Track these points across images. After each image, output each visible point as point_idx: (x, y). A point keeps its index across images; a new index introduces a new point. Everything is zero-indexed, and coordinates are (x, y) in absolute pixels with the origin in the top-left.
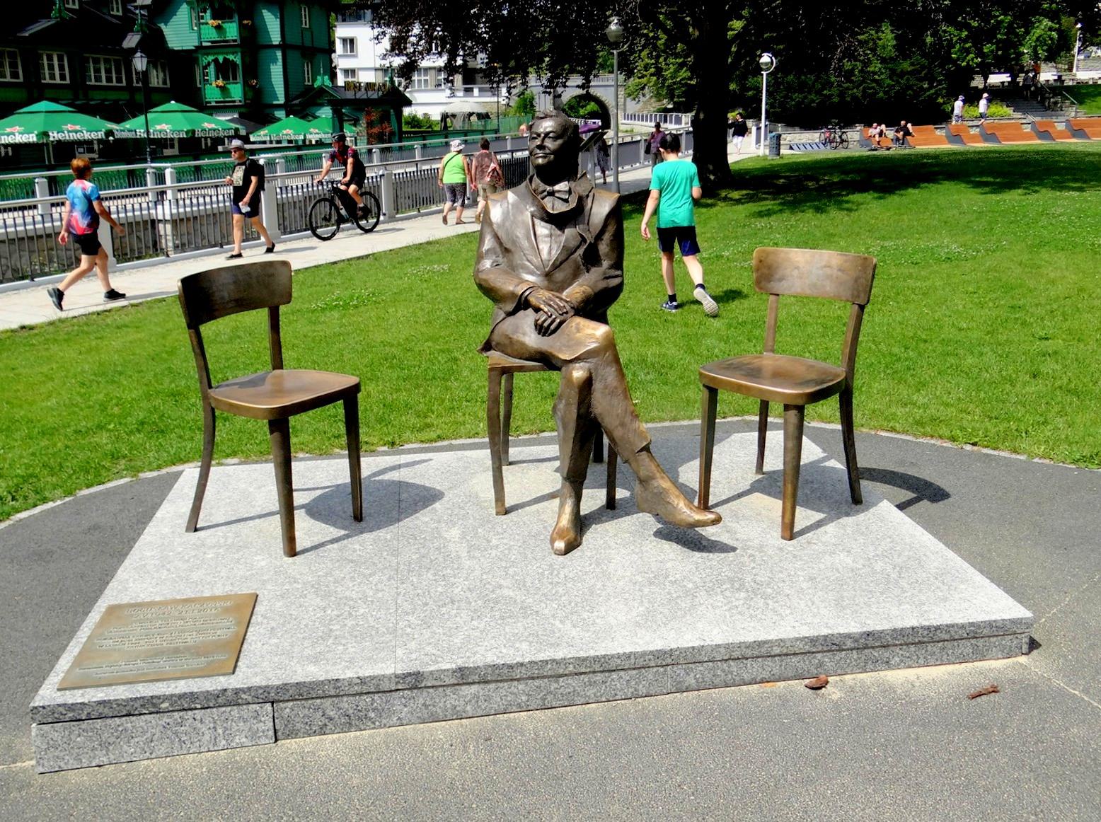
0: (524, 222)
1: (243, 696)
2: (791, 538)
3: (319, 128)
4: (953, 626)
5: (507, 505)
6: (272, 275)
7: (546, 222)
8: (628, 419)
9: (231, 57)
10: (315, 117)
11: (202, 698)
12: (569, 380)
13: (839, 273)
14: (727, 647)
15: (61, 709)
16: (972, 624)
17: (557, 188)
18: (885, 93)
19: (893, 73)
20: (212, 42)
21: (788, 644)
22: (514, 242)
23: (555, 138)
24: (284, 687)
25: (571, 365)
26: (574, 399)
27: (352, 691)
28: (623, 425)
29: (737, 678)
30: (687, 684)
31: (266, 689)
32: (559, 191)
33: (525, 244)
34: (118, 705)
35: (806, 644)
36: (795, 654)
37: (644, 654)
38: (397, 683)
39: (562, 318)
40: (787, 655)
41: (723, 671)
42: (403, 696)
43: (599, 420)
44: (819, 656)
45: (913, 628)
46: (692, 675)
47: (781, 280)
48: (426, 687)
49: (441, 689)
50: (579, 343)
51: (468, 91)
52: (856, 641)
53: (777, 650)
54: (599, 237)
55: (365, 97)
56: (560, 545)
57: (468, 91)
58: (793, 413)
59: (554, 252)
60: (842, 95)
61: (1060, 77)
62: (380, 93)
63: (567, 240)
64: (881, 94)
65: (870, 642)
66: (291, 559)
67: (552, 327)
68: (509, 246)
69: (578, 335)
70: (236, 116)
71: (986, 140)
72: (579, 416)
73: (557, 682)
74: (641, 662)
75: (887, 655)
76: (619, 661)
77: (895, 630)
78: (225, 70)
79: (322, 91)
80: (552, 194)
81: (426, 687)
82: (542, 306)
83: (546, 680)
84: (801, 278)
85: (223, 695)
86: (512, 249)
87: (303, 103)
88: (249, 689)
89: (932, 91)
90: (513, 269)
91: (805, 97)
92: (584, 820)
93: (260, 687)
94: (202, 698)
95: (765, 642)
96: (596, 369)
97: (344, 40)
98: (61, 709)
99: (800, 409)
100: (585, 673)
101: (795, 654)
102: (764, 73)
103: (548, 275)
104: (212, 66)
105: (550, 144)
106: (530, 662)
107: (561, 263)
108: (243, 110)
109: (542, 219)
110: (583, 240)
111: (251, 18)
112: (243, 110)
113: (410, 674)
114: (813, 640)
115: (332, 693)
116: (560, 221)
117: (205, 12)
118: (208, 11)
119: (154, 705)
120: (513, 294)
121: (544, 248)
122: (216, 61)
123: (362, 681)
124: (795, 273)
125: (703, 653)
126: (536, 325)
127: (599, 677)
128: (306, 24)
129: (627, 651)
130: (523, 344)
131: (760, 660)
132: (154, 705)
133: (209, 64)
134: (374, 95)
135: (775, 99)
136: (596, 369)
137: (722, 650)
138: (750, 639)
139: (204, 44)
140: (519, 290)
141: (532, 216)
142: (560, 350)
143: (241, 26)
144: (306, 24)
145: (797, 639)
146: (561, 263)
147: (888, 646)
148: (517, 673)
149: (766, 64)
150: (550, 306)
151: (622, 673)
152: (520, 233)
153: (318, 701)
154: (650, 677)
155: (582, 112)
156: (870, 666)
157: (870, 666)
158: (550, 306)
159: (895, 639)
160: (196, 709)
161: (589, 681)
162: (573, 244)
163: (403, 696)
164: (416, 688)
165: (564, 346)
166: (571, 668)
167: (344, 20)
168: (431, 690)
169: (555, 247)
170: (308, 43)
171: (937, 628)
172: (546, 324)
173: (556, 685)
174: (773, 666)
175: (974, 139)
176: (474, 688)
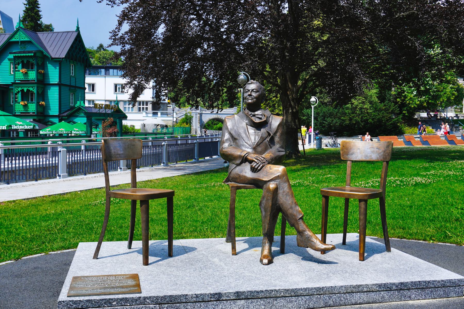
0: (243, 127)
1: (148, 301)
2: (363, 260)
3: (79, 126)
4: (435, 281)
5: (237, 251)
6: (134, 145)
7: (253, 127)
8: (293, 206)
9: (31, 89)
10: (75, 123)
11: (130, 301)
12: (268, 189)
13: (377, 150)
14: (346, 287)
15: (71, 303)
16: (442, 281)
17: (256, 113)
18: (373, 119)
19: (376, 109)
20: (21, 81)
21: (370, 287)
22: (239, 135)
23: (256, 92)
24: (164, 297)
25: (268, 183)
26: (270, 198)
27: (192, 300)
28: (291, 208)
29: (349, 302)
30: (329, 303)
31: (157, 298)
32: (257, 115)
33: (244, 135)
34: (95, 302)
35: (377, 287)
36: (373, 291)
37: (312, 289)
38: (211, 298)
39: (263, 164)
40: (369, 291)
41: (344, 298)
42: (213, 304)
43: (281, 206)
44: (382, 293)
45: (419, 282)
46: (331, 299)
47: (352, 154)
48: (223, 300)
49: (229, 301)
50: (272, 174)
51: (155, 114)
52: (397, 286)
53: (365, 289)
54: (275, 133)
55: (104, 112)
56: (265, 261)
57: (155, 114)
58: (363, 203)
59: (256, 139)
60: (351, 119)
61: (457, 115)
62: (112, 110)
63: (262, 134)
64: (370, 120)
65: (403, 287)
66: (147, 266)
67: (259, 168)
68: (236, 137)
69: (271, 171)
70: (32, 120)
71: (423, 144)
72: (272, 204)
73: (276, 300)
74: (311, 293)
75: (409, 293)
76: (302, 292)
77: (412, 282)
78: (26, 96)
79: (79, 109)
80: (254, 116)
81: (223, 300)
82: (254, 159)
83: (272, 299)
84: (361, 153)
85: (139, 300)
86: (238, 138)
87: (68, 114)
88: (150, 297)
89: (396, 119)
90: (238, 146)
91: (332, 121)
92: (311, 306)
93: (154, 297)
94: (130, 301)
95: (361, 285)
96: (279, 184)
97: (89, 85)
98: (71, 303)
99: (366, 201)
100: (288, 297)
101: (373, 291)
102: (313, 106)
103: (254, 149)
104: (20, 93)
105: (254, 94)
106: (266, 291)
107: (260, 144)
108: (35, 118)
109: (251, 126)
110: (269, 134)
111: (43, 69)
112: (35, 118)
113: (216, 294)
114: (380, 286)
115: (184, 301)
116: (258, 126)
117: (19, 65)
118: (20, 65)
119: (110, 303)
120: (240, 156)
121: (253, 138)
122: (22, 91)
123: (197, 296)
124: (358, 151)
125: (336, 289)
126: (251, 168)
127: (294, 299)
128: (72, 74)
129: (305, 287)
130: (245, 177)
131: (359, 293)
132: (110, 303)
133: (18, 92)
134: (109, 111)
135: (317, 120)
136: (279, 184)
137: (343, 288)
138: (355, 284)
139: (17, 82)
140: (243, 154)
141: (247, 124)
142: (263, 177)
143: (38, 73)
144: (72, 74)
145: (373, 285)
146: (260, 144)
147: (410, 289)
148: (261, 295)
149: (313, 102)
150: (258, 159)
151: (303, 297)
152: (241, 131)
153: (178, 304)
154: (314, 299)
155: (215, 127)
156: (403, 299)
157: (403, 299)
158: (258, 159)
159: (413, 286)
160: (127, 306)
161: (290, 301)
162: (265, 136)
163: (213, 304)
164: (219, 300)
165: (265, 175)
166: (282, 294)
167: (89, 74)
168: (225, 302)
169: (257, 137)
170: (73, 84)
171: (429, 282)
172: (256, 167)
173: (276, 302)
174: (364, 297)
175: (417, 143)
176: (243, 301)
